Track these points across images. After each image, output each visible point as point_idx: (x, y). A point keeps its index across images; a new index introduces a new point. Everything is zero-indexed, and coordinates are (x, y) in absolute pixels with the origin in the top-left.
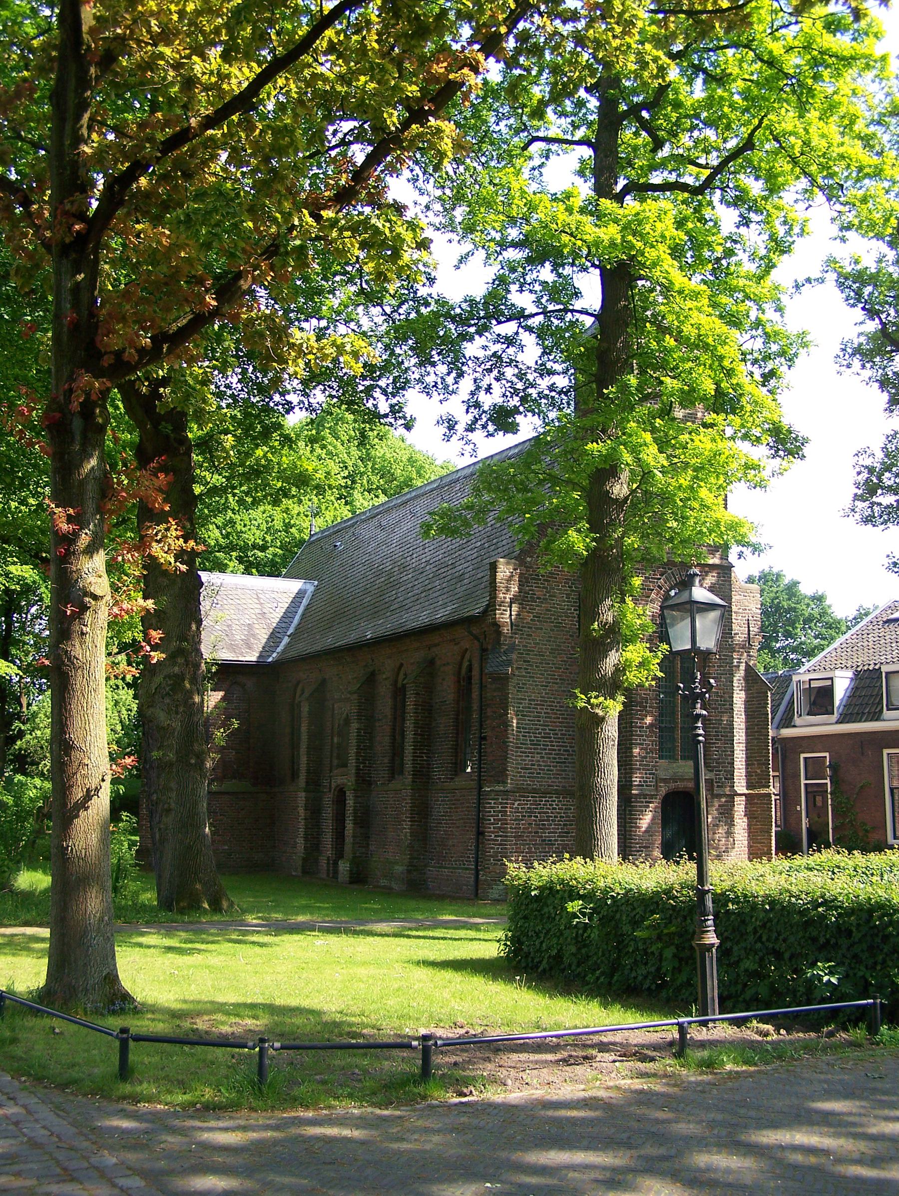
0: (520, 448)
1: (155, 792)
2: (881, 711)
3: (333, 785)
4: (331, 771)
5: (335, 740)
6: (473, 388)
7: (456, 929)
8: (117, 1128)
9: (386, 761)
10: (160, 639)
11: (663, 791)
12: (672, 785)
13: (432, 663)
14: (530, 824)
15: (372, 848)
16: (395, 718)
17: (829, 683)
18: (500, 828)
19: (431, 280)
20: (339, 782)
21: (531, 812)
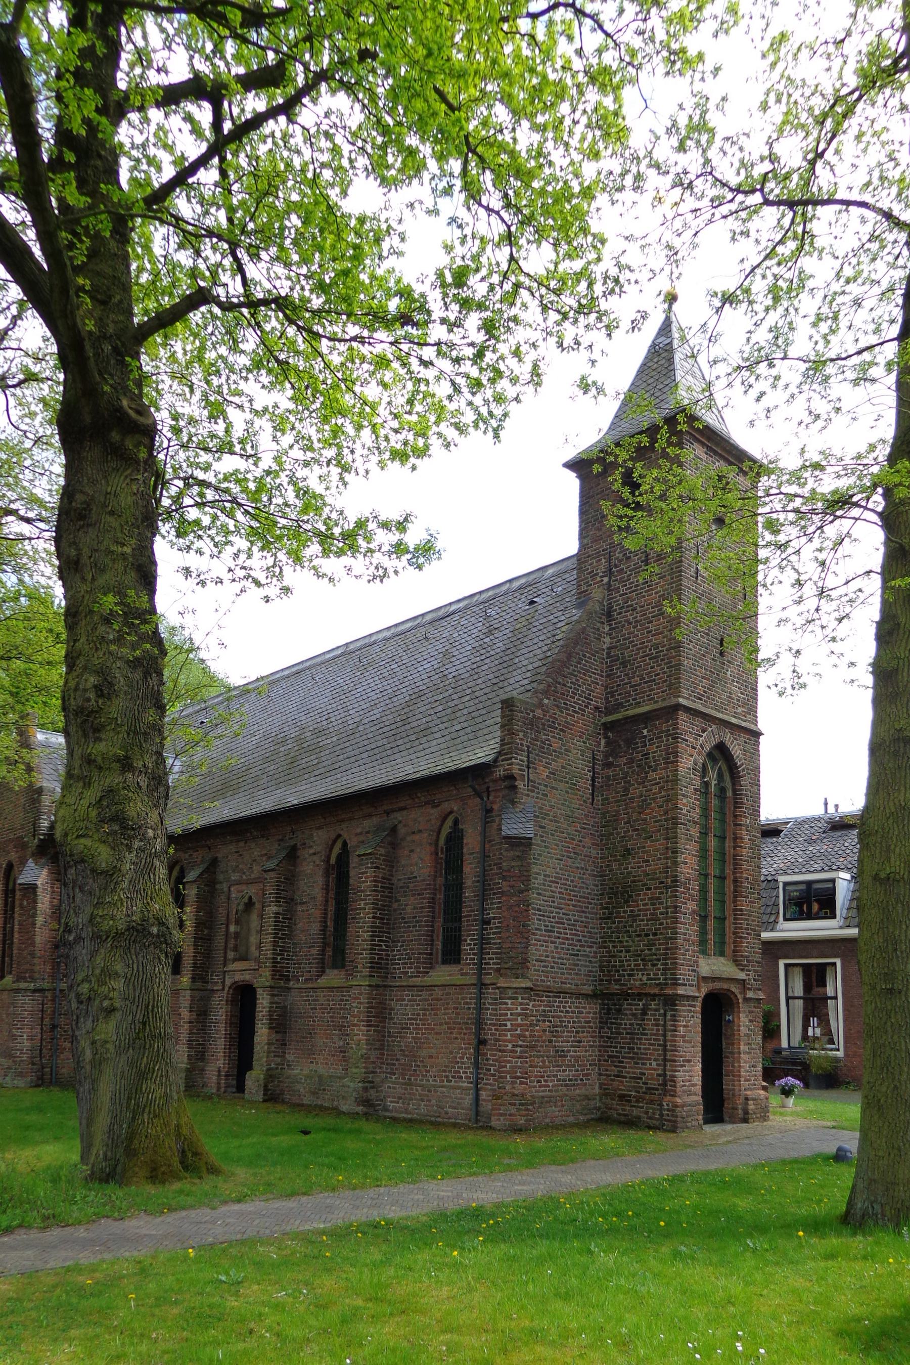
0: (565, 564)
1: (86, 980)
2: (776, 922)
3: (228, 982)
4: (225, 965)
5: (232, 928)
6: (731, 285)
7: (550, 1203)
8: (43, 249)
9: (314, 951)
10: (104, 54)
11: (704, 991)
12: (711, 986)
13: (394, 830)
14: (544, 1031)
15: (290, 1057)
16: (327, 901)
17: (831, 885)
18: (519, 1036)
19: (624, 118)
20: (238, 977)
21: (544, 1014)
